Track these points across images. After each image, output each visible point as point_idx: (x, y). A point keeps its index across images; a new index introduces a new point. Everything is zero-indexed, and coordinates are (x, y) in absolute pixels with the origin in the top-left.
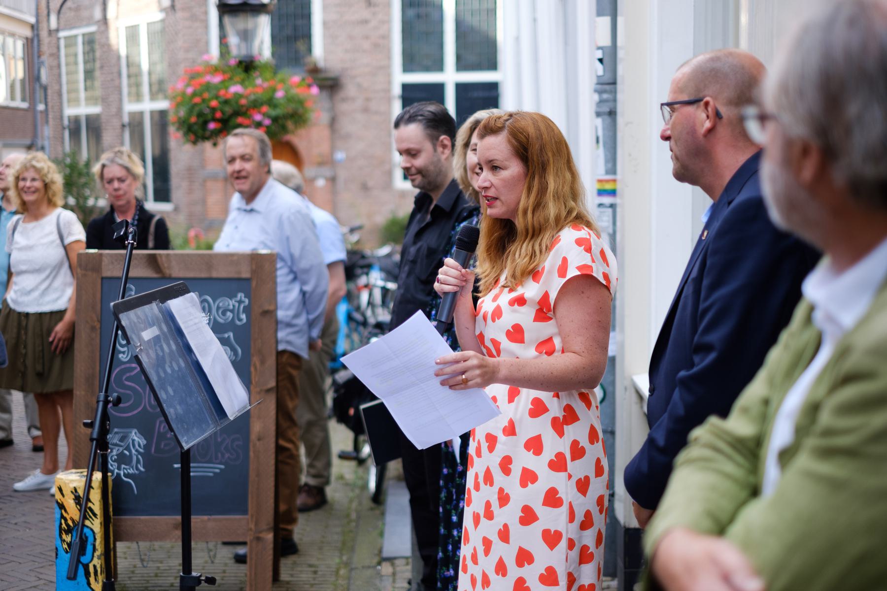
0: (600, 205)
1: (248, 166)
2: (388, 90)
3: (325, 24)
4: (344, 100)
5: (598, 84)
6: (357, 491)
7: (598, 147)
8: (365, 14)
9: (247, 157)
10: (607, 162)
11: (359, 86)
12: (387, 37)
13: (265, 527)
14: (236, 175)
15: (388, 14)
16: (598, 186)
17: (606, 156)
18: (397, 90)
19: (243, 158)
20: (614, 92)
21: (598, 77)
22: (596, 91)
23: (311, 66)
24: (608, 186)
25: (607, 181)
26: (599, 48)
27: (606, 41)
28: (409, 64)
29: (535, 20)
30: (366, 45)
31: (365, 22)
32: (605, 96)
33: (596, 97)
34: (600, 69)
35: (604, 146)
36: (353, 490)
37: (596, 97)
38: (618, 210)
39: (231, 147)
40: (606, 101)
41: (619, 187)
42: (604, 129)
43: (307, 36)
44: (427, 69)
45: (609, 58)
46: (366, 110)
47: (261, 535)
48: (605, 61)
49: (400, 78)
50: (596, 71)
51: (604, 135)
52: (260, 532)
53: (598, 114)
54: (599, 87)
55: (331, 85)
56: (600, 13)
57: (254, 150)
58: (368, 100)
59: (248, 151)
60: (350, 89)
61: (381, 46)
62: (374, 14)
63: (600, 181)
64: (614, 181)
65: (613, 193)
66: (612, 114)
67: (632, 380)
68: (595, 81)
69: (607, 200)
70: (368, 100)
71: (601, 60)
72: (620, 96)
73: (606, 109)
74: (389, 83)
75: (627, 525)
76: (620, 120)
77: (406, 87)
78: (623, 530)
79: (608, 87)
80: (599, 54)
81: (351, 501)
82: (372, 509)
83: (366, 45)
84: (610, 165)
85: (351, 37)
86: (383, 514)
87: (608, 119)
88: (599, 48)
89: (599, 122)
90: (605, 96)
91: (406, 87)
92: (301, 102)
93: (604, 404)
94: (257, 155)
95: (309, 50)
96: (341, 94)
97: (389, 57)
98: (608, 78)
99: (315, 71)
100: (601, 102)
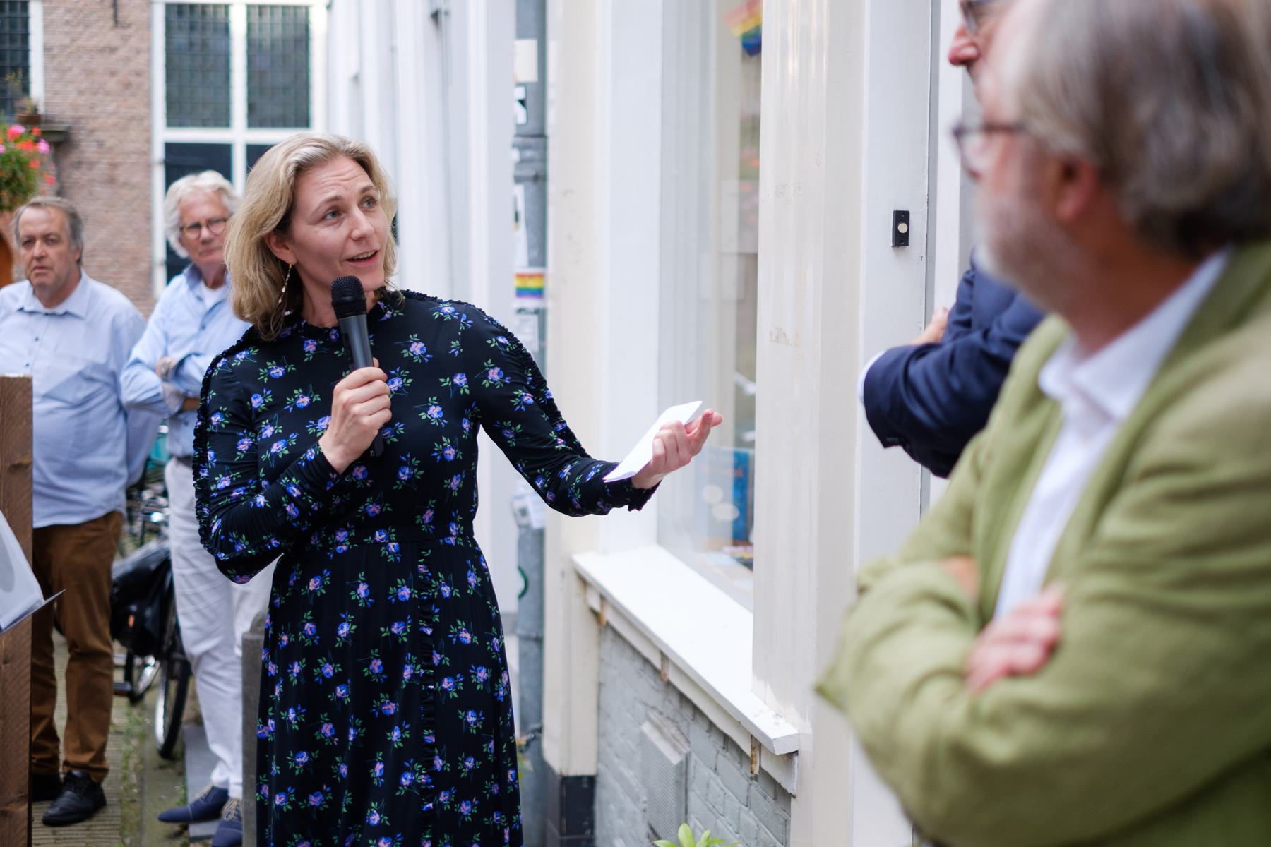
0: (520, 311)
1: (52, 252)
2: (147, 153)
3: (47, 49)
4: (79, 165)
5: (518, 135)
6: (134, 742)
7: (517, 228)
8: (112, 38)
9: (52, 237)
10: (530, 248)
11: (101, 144)
12: (144, 73)
13: (13, 795)
14: (35, 263)
15: (149, 40)
16: (517, 283)
17: (529, 240)
18: (159, 153)
19: (47, 239)
20: (544, 149)
21: (518, 126)
22: (514, 146)
23: (28, 112)
24: (533, 284)
25: (531, 276)
26: (519, 84)
27: (530, 75)
28: (176, 116)
29: (393, 50)
30: (112, 84)
31: (113, 50)
32: (529, 154)
33: (515, 155)
34: (521, 114)
35: (527, 225)
36: (128, 743)
37: (515, 155)
38: (550, 319)
39: (28, 223)
40: (531, 160)
41: (550, 286)
42: (526, 201)
43: (23, 68)
44: (204, 123)
45: (535, 99)
46: (111, 181)
47: (8, 808)
48: (528, 103)
49: (163, 134)
50: (515, 118)
51: (527, 210)
52: (8, 804)
53: (518, 180)
54: (520, 140)
55: (62, 141)
56: (521, 34)
57: (62, 227)
58: (114, 166)
59: (54, 228)
60: (88, 149)
61: (135, 85)
62: (125, 39)
63: (521, 276)
64: (541, 276)
65: (539, 293)
66: (540, 179)
67: (572, 562)
68: (513, 131)
69: (531, 303)
70: (114, 166)
71: (522, 102)
72: (553, 154)
73: (529, 171)
74: (149, 141)
75: (565, 773)
76: (553, 188)
77: (170, 148)
78: (557, 784)
79: (532, 141)
80: (520, 93)
81: (127, 757)
82: (161, 767)
83: (112, 84)
84: (535, 253)
85: (89, 73)
86: (182, 773)
87: (532, 188)
88: (519, 84)
89: (519, 190)
90: (529, 154)
91: (170, 148)
92: (22, 164)
93: (525, 598)
94: (65, 236)
95: (26, 89)
96: (74, 157)
97: (149, 104)
98: (532, 128)
99: (33, 119)
100: (523, 161)
